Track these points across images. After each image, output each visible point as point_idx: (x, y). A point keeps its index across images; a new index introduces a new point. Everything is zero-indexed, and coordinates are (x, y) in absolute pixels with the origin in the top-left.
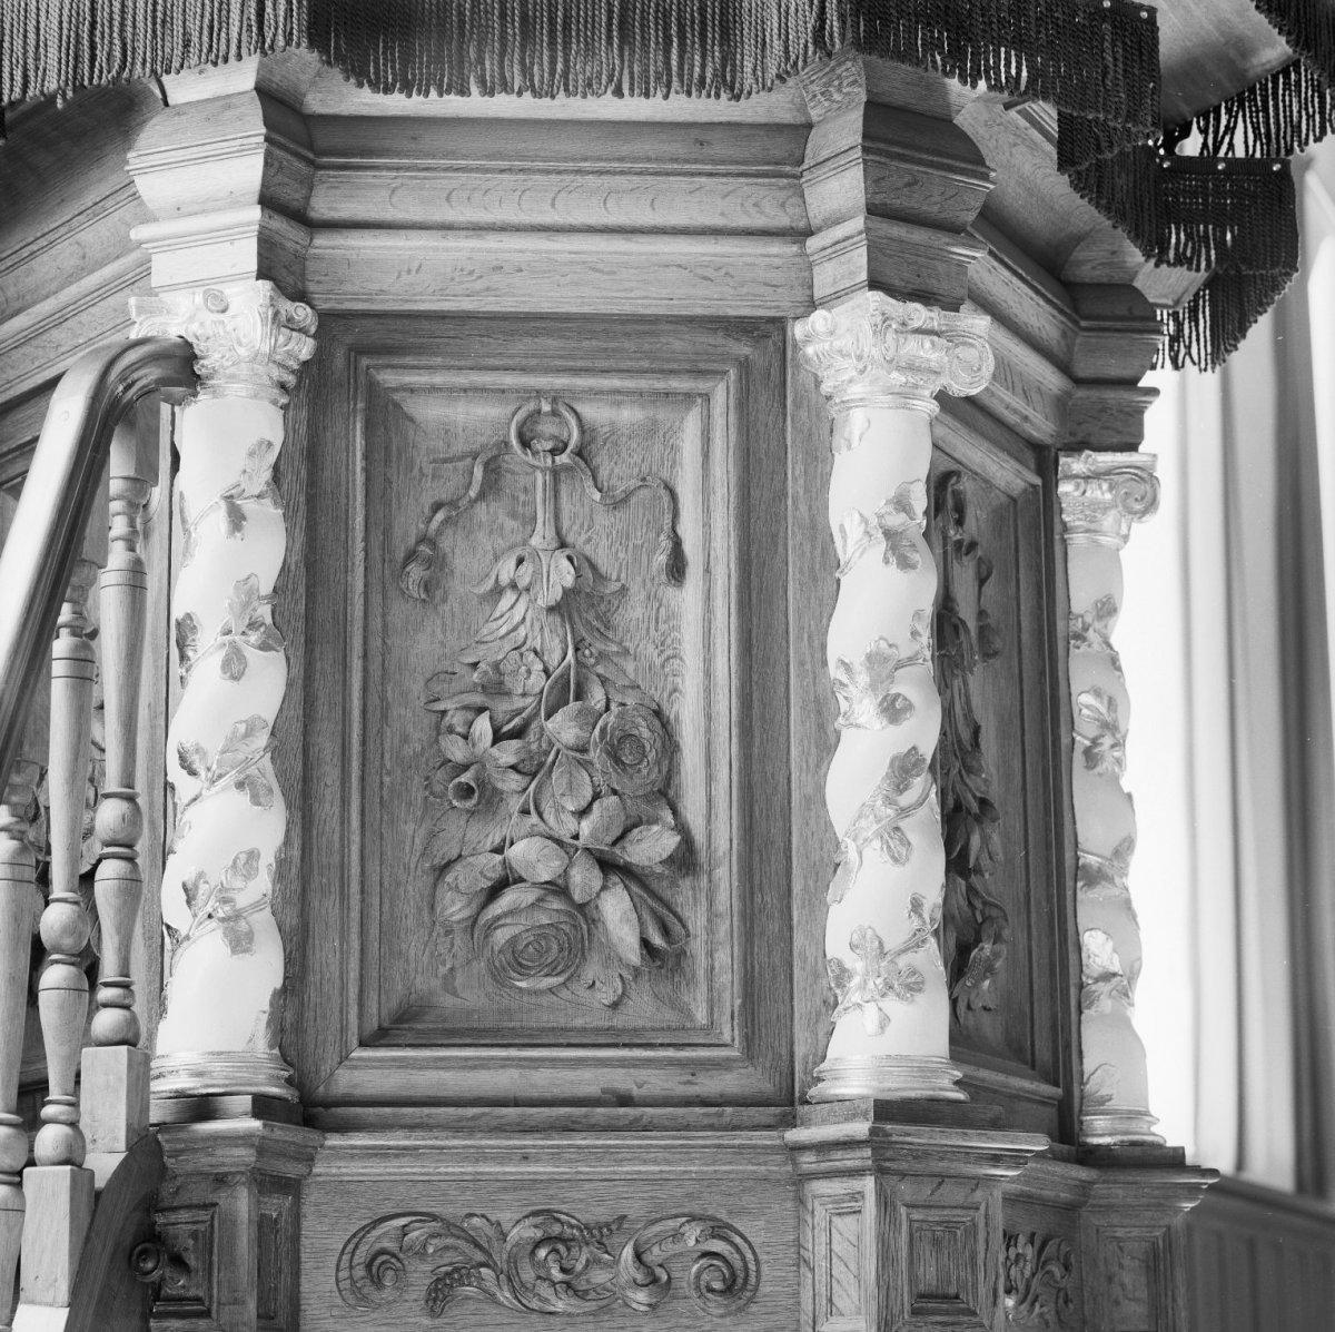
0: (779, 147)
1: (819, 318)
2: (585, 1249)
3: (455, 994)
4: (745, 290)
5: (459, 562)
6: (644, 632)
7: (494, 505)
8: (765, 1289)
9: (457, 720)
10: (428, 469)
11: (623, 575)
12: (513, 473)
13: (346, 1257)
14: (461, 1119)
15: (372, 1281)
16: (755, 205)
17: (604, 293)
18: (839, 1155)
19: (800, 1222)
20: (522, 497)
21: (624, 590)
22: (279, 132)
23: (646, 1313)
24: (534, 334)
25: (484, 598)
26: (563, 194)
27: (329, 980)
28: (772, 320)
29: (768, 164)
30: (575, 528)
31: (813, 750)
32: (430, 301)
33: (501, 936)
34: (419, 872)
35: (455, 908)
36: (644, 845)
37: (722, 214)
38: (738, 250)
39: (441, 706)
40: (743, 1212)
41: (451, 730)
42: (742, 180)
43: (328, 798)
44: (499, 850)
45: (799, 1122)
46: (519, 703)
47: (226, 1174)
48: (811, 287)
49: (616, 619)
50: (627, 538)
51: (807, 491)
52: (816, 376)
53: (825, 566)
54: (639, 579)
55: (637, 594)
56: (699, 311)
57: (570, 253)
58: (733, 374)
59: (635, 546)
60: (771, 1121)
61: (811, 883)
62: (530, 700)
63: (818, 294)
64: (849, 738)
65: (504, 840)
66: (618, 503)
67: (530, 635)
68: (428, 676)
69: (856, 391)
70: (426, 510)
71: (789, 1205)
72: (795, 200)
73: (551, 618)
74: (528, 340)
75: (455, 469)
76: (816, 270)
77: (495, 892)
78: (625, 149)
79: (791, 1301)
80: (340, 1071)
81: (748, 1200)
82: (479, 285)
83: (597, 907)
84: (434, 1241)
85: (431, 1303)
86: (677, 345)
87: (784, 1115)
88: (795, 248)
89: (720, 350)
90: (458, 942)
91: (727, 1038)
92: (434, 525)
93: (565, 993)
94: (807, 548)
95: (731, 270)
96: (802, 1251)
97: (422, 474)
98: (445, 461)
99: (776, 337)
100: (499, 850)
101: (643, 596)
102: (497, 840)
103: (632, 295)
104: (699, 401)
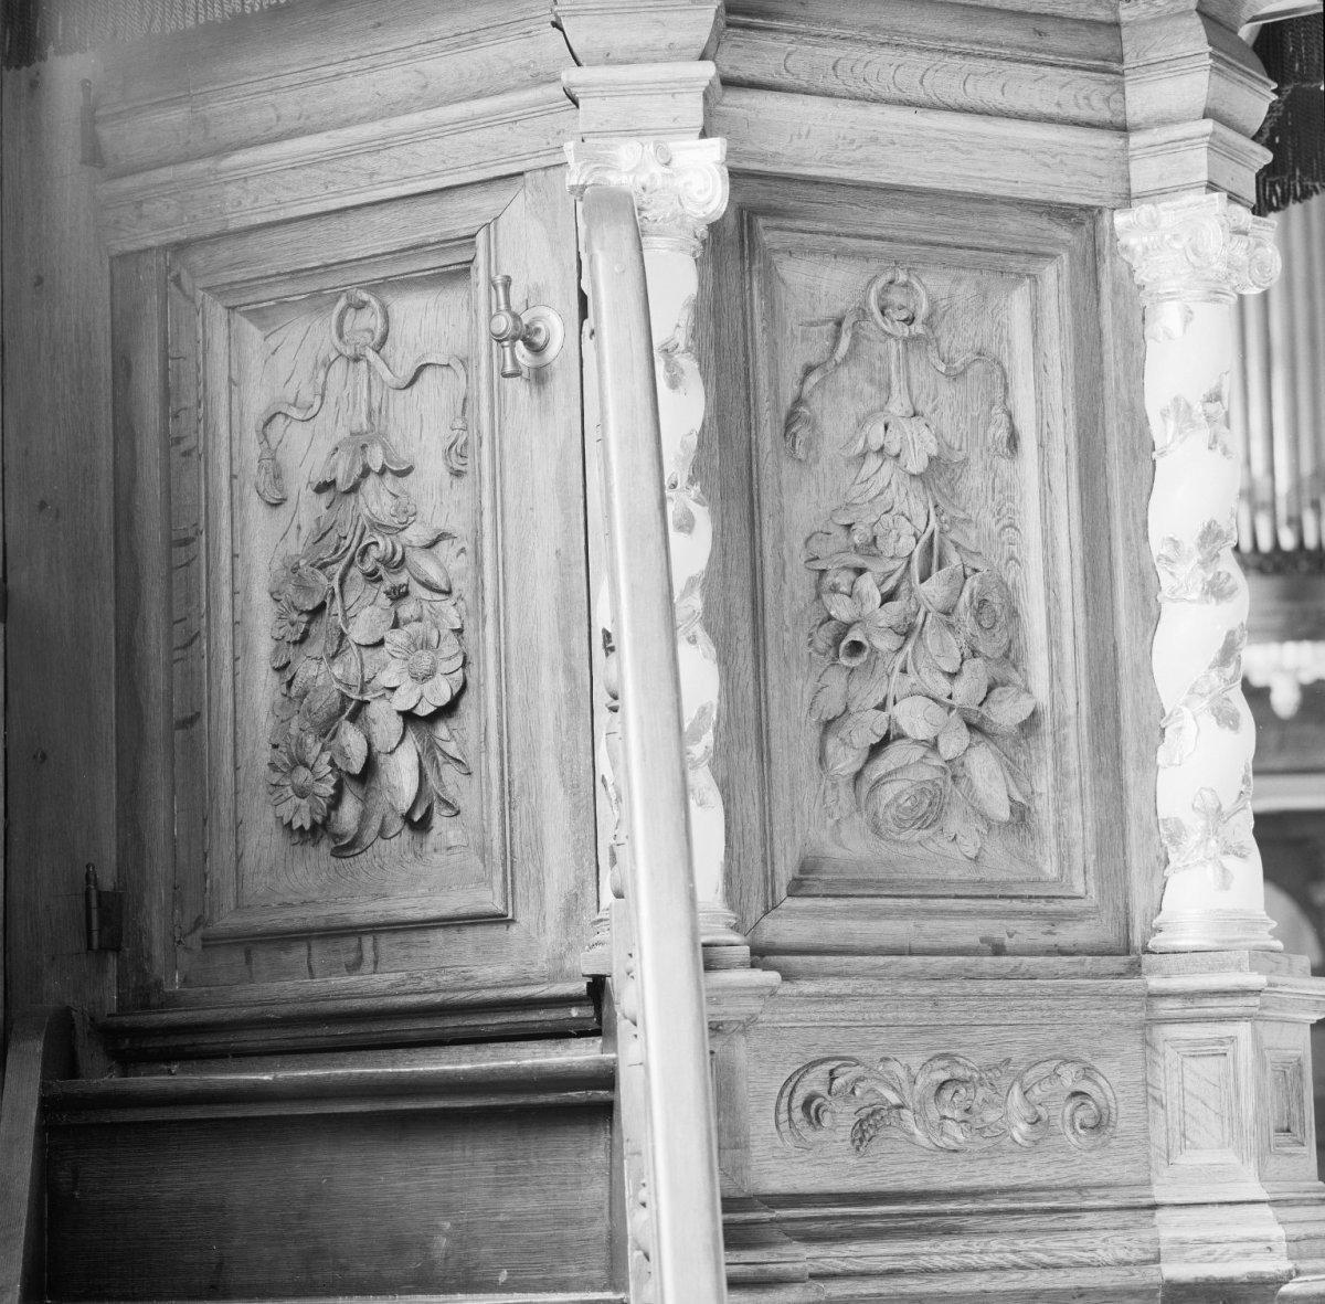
0: (1103, 43)
1: (1142, 211)
2: (980, 1090)
3: (841, 845)
4: (1076, 178)
5: (827, 424)
6: (982, 501)
7: (854, 370)
8: (1122, 1125)
9: (843, 580)
10: (798, 331)
11: (964, 445)
12: (869, 340)
13: (785, 1101)
14: (874, 967)
15: (810, 1123)
16: (1087, 98)
17: (963, 172)
18: (1215, 1002)
19: (1148, 1063)
20: (878, 364)
21: (965, 462)
22: (1221, 50)
23: (1029, 1149)
24: (894, 206)
25: (849, 461)
26: (931, 73)
27: (750, 830)
28: (1088, 209)
29: (1095, 59)
30: (923, 396)
31: (1140, 622)
32: (818, 166)
33: (888, 792)
34: (808, 727)
35: (845, 760)
36: (1005, 706)
37: (1059, 105)
38: (1073, 140)
39: (820, 565)
40: (1102, 1054)
41: (834, 589)
42: (1080, 73)
43: (741, 652)
44: (882, 707)
45: (1144, 970)
46: (891, 566)
47: (722, 1023)
48: (1128, 180)
49: (959, 487)
50: (966, 410)
51: (1127, 374)
52: (1130, 266)
53: (1142, 450)
54: (977, 450)
55: (976, 466)
56: (1038, 196)
57: (938, 130)
58: (1065, 256)
59: (972, 419)
60: (1122, 969)
61: (1143, 746)
62: (897, 563)
63: (1136, 188)
64: (1169, 612)
65: (885, 699)
66: (955, 376)
67: (897, 499)
68: (807, 535)
69: (1172, 285)
70: (798, 372)
71: (1138, 1047)
72: (1118, 96)
73: (914, 484)
74: (890, 212)
75: (820, 332)
76: (1133, 165)
77: (876, 750)
78: (980, 33)
79: (1142, 1135)
80: (764, 920)
81: (1106, 1044)
82: (858, 155)
83: (963, 765)
84: (861, 1084)
85: (857, 1143)
86: (1013, 226)
87: (1132, 964)
88: (1121, 142)
89: (1046, 234)
90: (842, 794)
91: (1079, 889)
92: (808, 387)
93: (931, 845)
94: (1128, 429)
95: (1064, 158)
96: (1150, 1090)
97: (794, 336)
98: (811, 324)
99: (1088, 224)
100: (882, 707)
101: (981, 465)
102: (880, 700)
103: (986, 175)
104: (1027, 281)
